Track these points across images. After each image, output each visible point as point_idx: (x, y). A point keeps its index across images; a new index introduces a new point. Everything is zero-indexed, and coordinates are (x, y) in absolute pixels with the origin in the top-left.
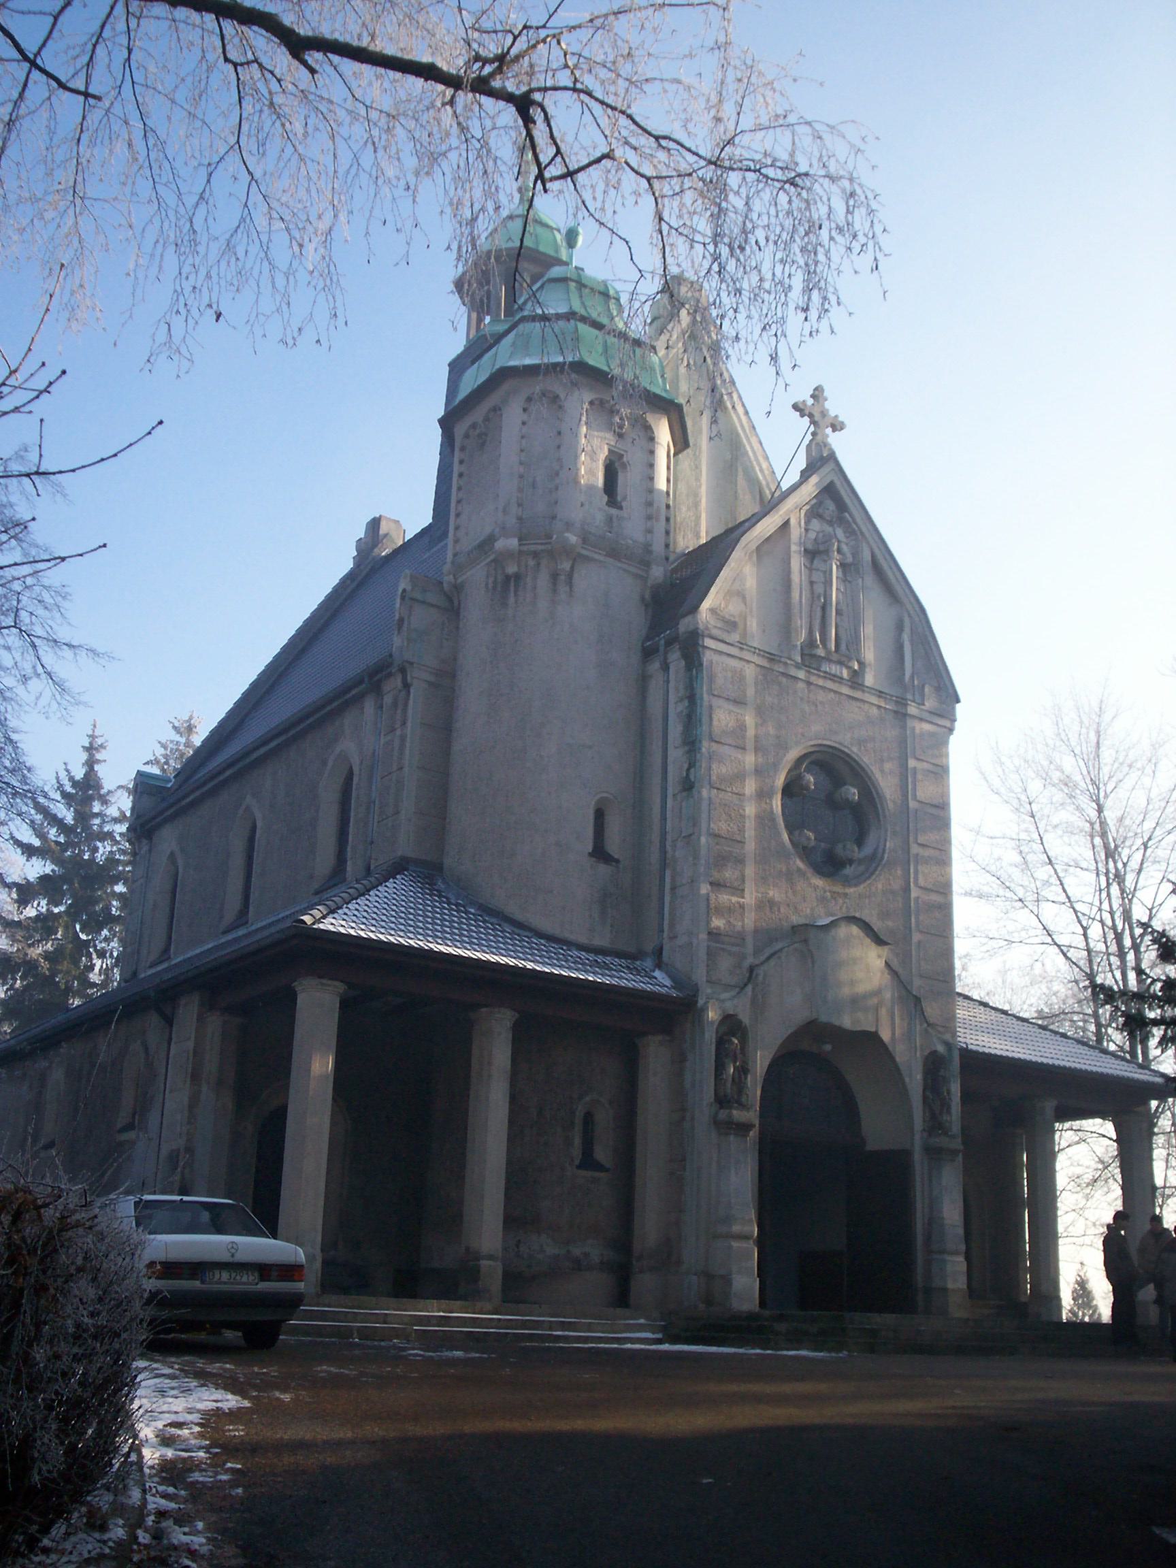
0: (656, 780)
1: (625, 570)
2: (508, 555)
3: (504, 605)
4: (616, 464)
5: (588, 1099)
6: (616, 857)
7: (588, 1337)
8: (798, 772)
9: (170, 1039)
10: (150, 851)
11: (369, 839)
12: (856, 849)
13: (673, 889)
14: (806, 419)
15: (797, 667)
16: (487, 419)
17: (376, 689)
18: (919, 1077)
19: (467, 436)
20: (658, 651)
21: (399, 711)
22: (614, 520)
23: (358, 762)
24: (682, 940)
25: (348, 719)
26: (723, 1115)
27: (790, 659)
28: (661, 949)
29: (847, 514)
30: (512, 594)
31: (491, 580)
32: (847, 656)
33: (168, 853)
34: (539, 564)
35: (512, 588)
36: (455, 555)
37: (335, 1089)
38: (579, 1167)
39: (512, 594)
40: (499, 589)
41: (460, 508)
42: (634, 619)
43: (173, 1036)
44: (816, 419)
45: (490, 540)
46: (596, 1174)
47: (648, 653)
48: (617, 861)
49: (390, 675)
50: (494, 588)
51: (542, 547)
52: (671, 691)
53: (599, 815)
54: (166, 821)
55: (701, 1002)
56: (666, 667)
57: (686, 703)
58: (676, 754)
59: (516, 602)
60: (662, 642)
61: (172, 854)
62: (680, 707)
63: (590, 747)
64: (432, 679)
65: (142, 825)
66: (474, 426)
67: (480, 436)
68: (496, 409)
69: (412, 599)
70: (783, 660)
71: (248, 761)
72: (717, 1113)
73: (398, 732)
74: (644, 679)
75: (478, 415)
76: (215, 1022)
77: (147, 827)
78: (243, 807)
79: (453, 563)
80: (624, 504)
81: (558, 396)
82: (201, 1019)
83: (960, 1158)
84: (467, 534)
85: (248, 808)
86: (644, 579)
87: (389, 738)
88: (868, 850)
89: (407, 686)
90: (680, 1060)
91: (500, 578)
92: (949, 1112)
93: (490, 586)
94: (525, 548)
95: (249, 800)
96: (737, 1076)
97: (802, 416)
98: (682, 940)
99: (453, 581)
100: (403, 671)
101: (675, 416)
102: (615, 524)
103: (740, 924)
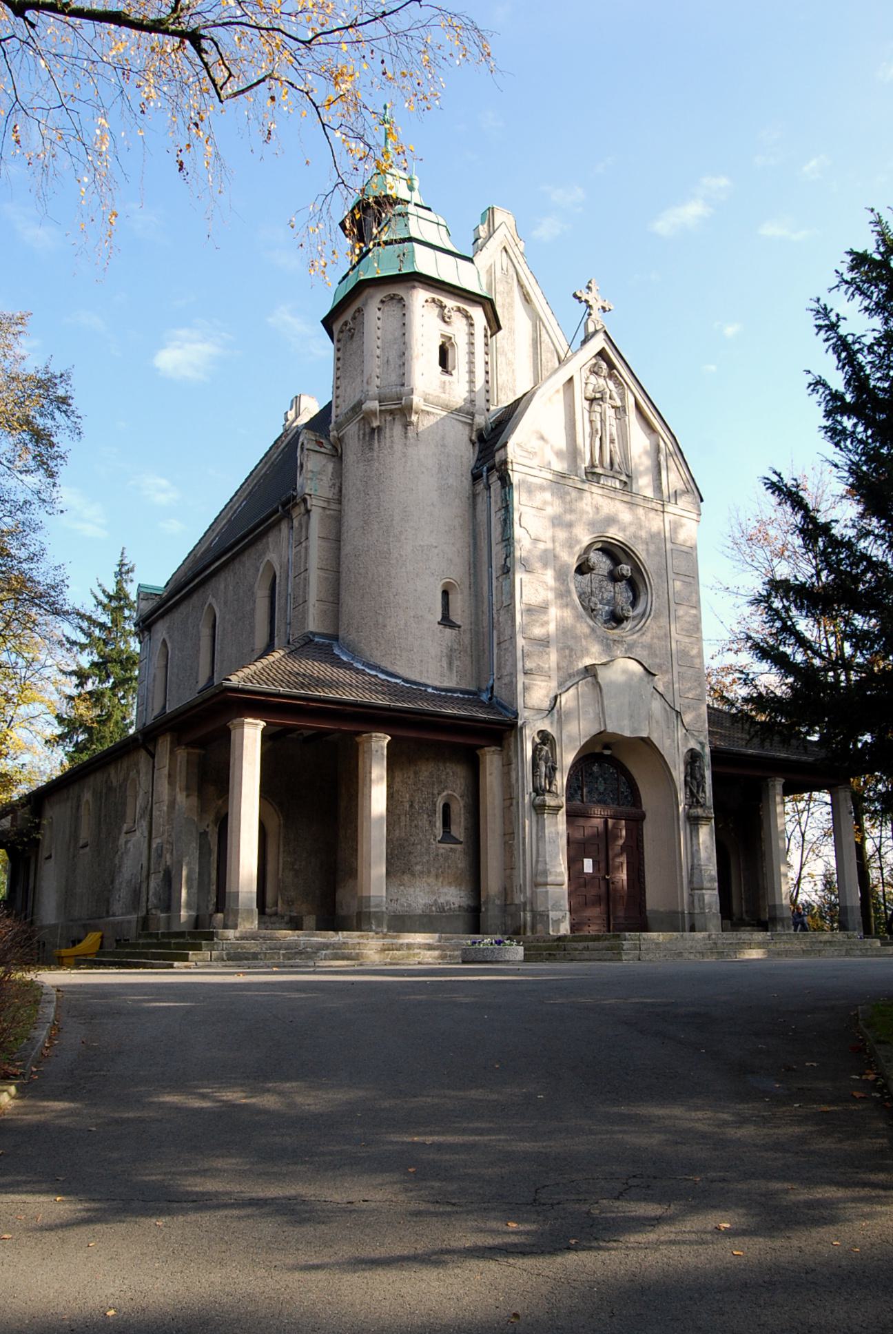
0: (485, 567)
1: (457, 420)
2: (373, 413)
3: (371, 449)
4: (447, 345)
5: (445, 793)
6: (459, 623)
7: (403, 976)
8: (586, 556)
9: (154, 767)
10: (150, 639)
11: (288, 621)
12: (631, 609)
13: (499, 644)
14: (583, 304)
15: (583, 482)
16: (354, 318)
17: (288, 515)
18: (682, 768)
19: (341, 331)
20: (482, 476)
21: (304, 530)
22: (447, 384)
23: (279, 567)
24: (506, 680)
25: (271, 539)
26: (538, 800)
27: (577, 476)
28: (492, 687)
29: (615, 371)
30: (376, 441)
31: (362, 432)
32: (619, 472)
33: (161, 640)
34: (394, 419)
35: (376, 437)
36: (337, 416)
37: (261, 796)
38: (439, 842)
39: (376, 441)
40: (367, 439)
41: (339, 382)
42: (467, 455)
43: (156, 764)
44: (590, 303)
45: (360, 403)
46: (453, 846)
47: (476, 477)
48: (459, 627)
49: (296, 504)
50: (364, 438)
51: (396, 406)
52: (493, 504)
53: (445, 593)
54: (162, 616)
55: (520, 722)
56: (488, 487)
57: (503, 511)
58: (497, 549)
59: (379, 446)
60: (485, 469)
61: (164, 641)
62: (499, 514)
63: (436, 547)
64: (325, 505)
65: (144, 621)
66: (346, 324)
67: (350, 330)
68: (359, 310)
69: (307, 449)
70: (572, 477)
71: (208, 572)
72: (535, 799)
73: (304, 544)
74: (474, 496)
75: (348, 315)
76: (182, 753)
77: (147, 623)
78: (208, 604)
79: (335, 422)
80: (453, 372)
81: (402, 298)
82: (172, 752)
83: (713, 821)
84: (344, 401)
85: (210, 606)
86: (471, 425)
87: (298, 549)
88: (639, 609)
89: (308, 512)
90: (507, 764)
91: (367, 430)
92: (704, 791)
93: (361, 437)
94: (383, 408)
95: (211, 600)
96: (548, 772)
97: (581, 302)
98: (506, 680)
99: (336, 435)
100: (305, 501)
101: (488, 307)
102: (447, 387)
103: (547, 666)
